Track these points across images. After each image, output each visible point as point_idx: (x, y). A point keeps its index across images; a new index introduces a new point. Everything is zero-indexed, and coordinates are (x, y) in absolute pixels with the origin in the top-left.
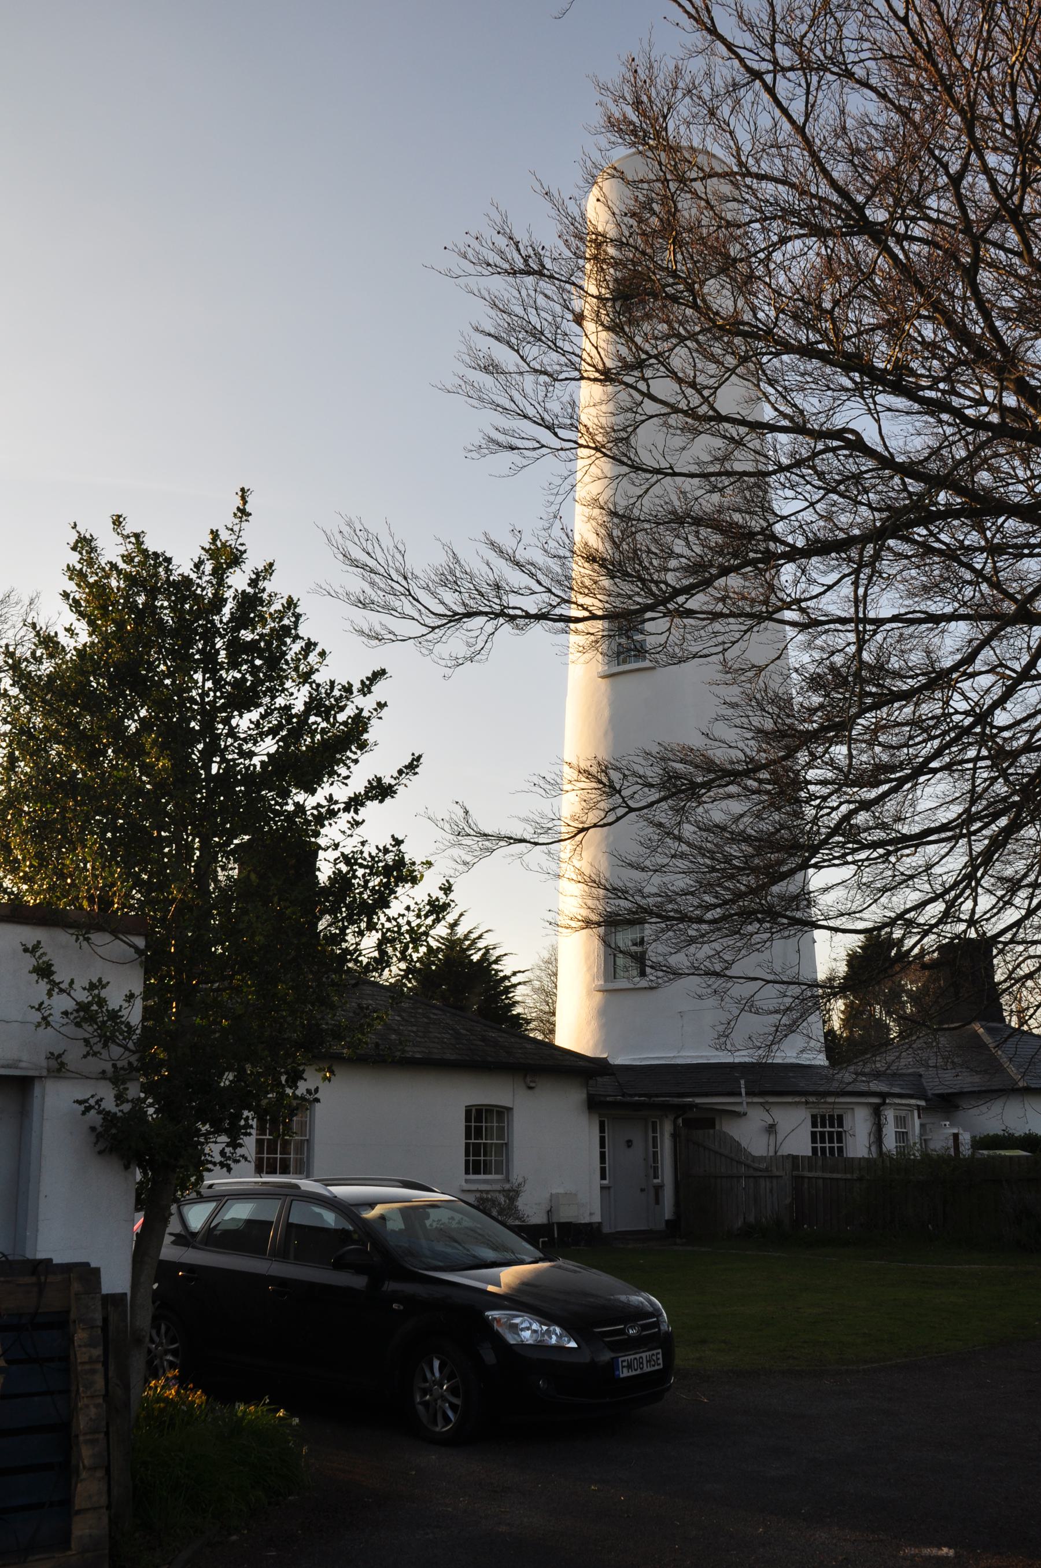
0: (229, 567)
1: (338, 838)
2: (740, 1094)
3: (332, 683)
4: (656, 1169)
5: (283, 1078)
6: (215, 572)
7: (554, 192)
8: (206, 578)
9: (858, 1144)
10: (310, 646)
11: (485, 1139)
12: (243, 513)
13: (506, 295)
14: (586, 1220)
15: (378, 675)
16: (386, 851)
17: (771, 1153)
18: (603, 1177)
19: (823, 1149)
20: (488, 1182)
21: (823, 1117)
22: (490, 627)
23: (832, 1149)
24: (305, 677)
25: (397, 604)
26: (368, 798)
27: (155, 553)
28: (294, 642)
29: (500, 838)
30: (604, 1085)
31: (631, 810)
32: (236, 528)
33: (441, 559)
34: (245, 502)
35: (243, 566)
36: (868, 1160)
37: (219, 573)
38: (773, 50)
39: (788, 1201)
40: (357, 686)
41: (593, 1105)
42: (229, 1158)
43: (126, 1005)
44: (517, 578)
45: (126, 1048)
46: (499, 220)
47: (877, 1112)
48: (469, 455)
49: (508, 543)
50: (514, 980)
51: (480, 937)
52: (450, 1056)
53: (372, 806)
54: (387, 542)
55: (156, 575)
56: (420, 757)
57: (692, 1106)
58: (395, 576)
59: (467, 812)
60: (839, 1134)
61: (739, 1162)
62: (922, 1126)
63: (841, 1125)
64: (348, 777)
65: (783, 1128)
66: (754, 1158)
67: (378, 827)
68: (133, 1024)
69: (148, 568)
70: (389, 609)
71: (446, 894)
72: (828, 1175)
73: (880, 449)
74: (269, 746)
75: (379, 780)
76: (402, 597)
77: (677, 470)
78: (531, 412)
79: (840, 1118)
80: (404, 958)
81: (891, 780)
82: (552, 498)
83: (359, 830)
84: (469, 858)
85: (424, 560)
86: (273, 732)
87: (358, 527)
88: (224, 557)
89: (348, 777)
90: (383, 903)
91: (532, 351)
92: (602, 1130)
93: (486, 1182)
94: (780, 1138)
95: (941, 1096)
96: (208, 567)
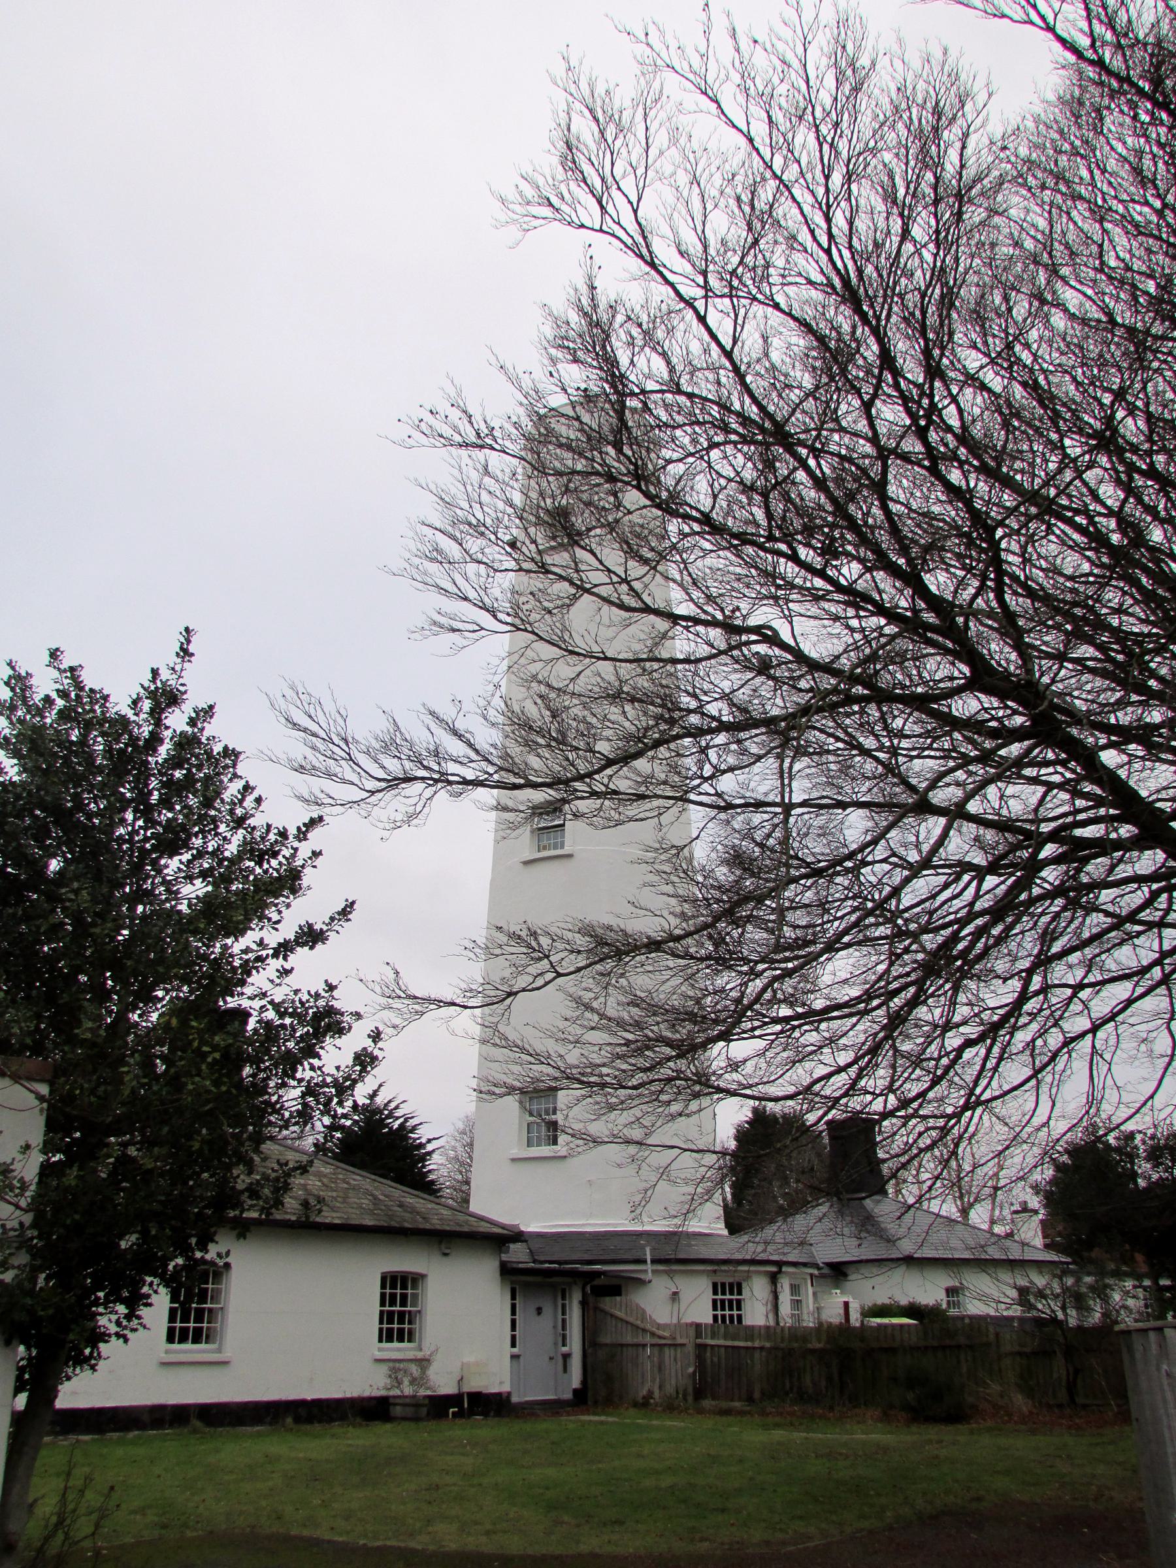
0: (168, 706)
1: (267, 986)
2: (645, 1262)
3: (269, 826)
4: (564, 1337)
5: (193, 1241)
6: (152, 712)
7: (509, 366)
8: (143, 716)
9: (756, 1314)
10: (247, 788)
11: (399, 1310)
12: (185, 653)
13: (453, 491)
14: (494, 1389)
15: (313, 823)
16: (317, 996)
17: (675, 1321)
18: (513, 1345)
19: (723, 1316)
20: (396, 1350)
21: (723, 1285)
22: (429, 792)
23: (731, 1316)
24: (239, 822)
25: (338, 769)
26: (298, 944)
27: (92, 690)
28: (231, 780)
29: (429, 1000)
30: (517, 1253)
31: (559, 975)
32: (178, 668)
33: (382, 726)
34: (189, 642)
35: (183, 707)
36: (767, 1328)
37: (157, 714)
38: (705, 277)
39: (691, 1370)
40: (292, 831)
41: (507, 1271)
42: (125, 1328)
43: (19, 1157)
44: (456, 747)
45: (17, 1206)
46: (453, 394)
47: (774, 1278)
48: (413, 636)
49: (447, 711)
50: (429, 1147)
51: (397, 1107)
52: (368, 1222)
53: (302, 952)
54: (329, 707)
55: (93, 711)
56: (353, 903)
57: (598, 1274)
58: (336, 740)
59: (397, 973)
60: (739, 1302)
61: (644, 1330)
62: (814, 1294)
63: (740, 1293)
64: (278, 922)
65: (686, 1297)
66: (659, 1326)
67: (309, 972)
68: (27, 1179)
69: (82, 706)
70: (330, 775)
71: (375, 1042)
72: (729, 1343)
73: (793, 644)
74: (198, 888)
75: (310, 926)
76: (343, 763)
77: (609, 655)
78: (472, 595)
79: (739, 1286)
80: (327, 1111)
81: (797, 958)
82: (490, 677)
83: (287, 980)
84: (397, 1021)
85: (366, 727)
86: (204, 874)
87: (301, 690)
88: (165, 698)
89: (278, 922)
90: (310, 1051)
91: (474, 545)
92: (513, 1298)
93: (399, 1350)
94: (683, 1306)
95: (830, 1265)
96: (147, 705)
